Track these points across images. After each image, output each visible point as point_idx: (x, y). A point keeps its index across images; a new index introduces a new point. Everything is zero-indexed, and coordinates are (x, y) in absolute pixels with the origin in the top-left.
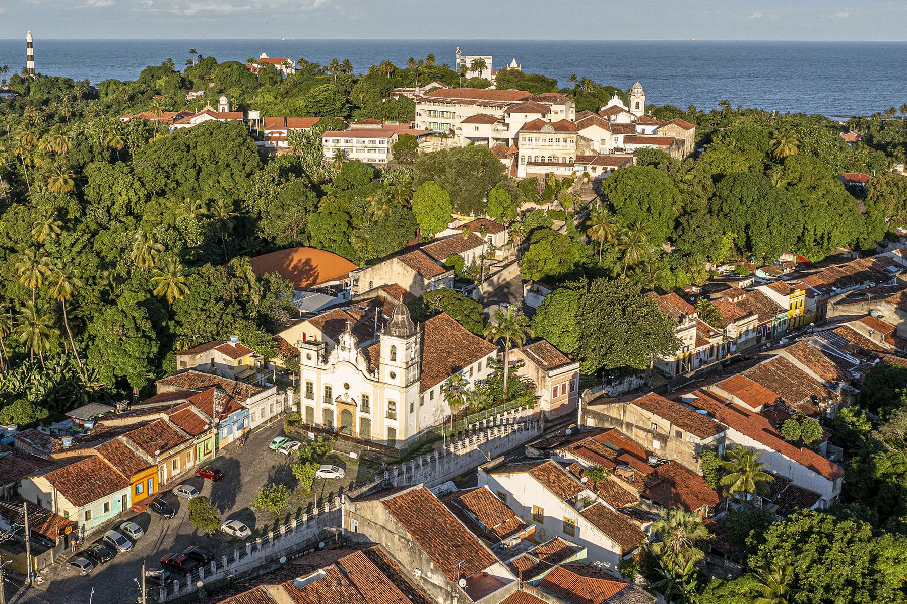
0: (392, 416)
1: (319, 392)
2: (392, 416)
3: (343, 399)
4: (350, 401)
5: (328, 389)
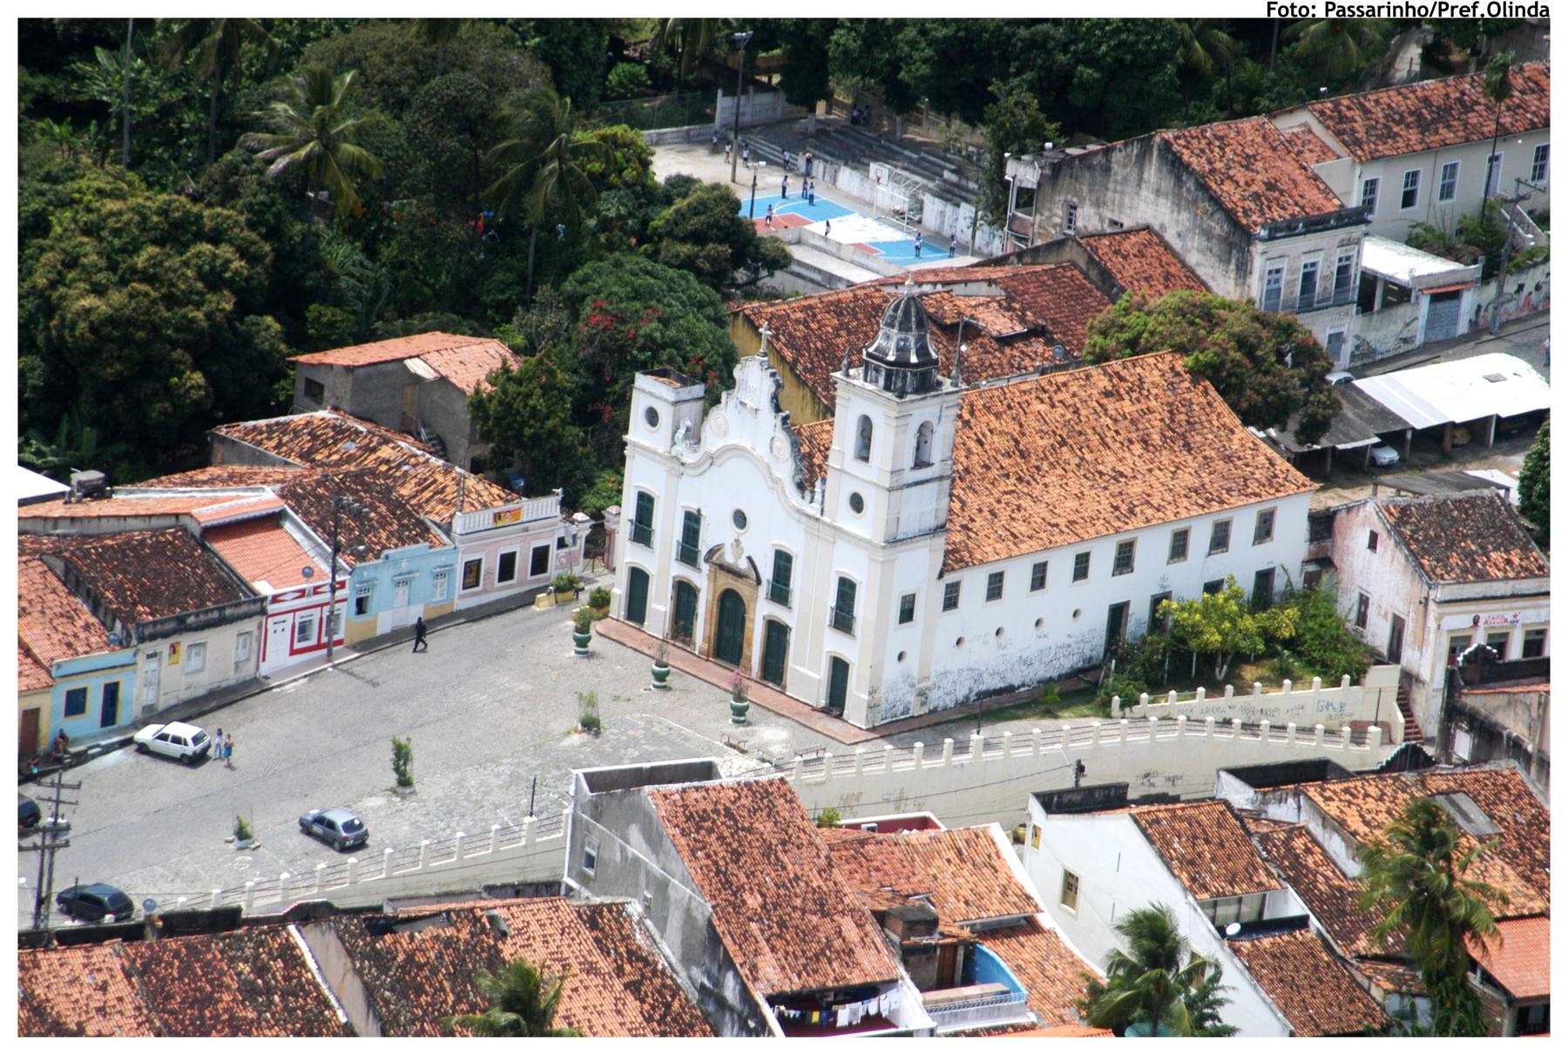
0: (843, 619)
1: (668, 529)
2: (843, 619)
3: (729, 558)
4: (743, 565)
5: (692, 522)
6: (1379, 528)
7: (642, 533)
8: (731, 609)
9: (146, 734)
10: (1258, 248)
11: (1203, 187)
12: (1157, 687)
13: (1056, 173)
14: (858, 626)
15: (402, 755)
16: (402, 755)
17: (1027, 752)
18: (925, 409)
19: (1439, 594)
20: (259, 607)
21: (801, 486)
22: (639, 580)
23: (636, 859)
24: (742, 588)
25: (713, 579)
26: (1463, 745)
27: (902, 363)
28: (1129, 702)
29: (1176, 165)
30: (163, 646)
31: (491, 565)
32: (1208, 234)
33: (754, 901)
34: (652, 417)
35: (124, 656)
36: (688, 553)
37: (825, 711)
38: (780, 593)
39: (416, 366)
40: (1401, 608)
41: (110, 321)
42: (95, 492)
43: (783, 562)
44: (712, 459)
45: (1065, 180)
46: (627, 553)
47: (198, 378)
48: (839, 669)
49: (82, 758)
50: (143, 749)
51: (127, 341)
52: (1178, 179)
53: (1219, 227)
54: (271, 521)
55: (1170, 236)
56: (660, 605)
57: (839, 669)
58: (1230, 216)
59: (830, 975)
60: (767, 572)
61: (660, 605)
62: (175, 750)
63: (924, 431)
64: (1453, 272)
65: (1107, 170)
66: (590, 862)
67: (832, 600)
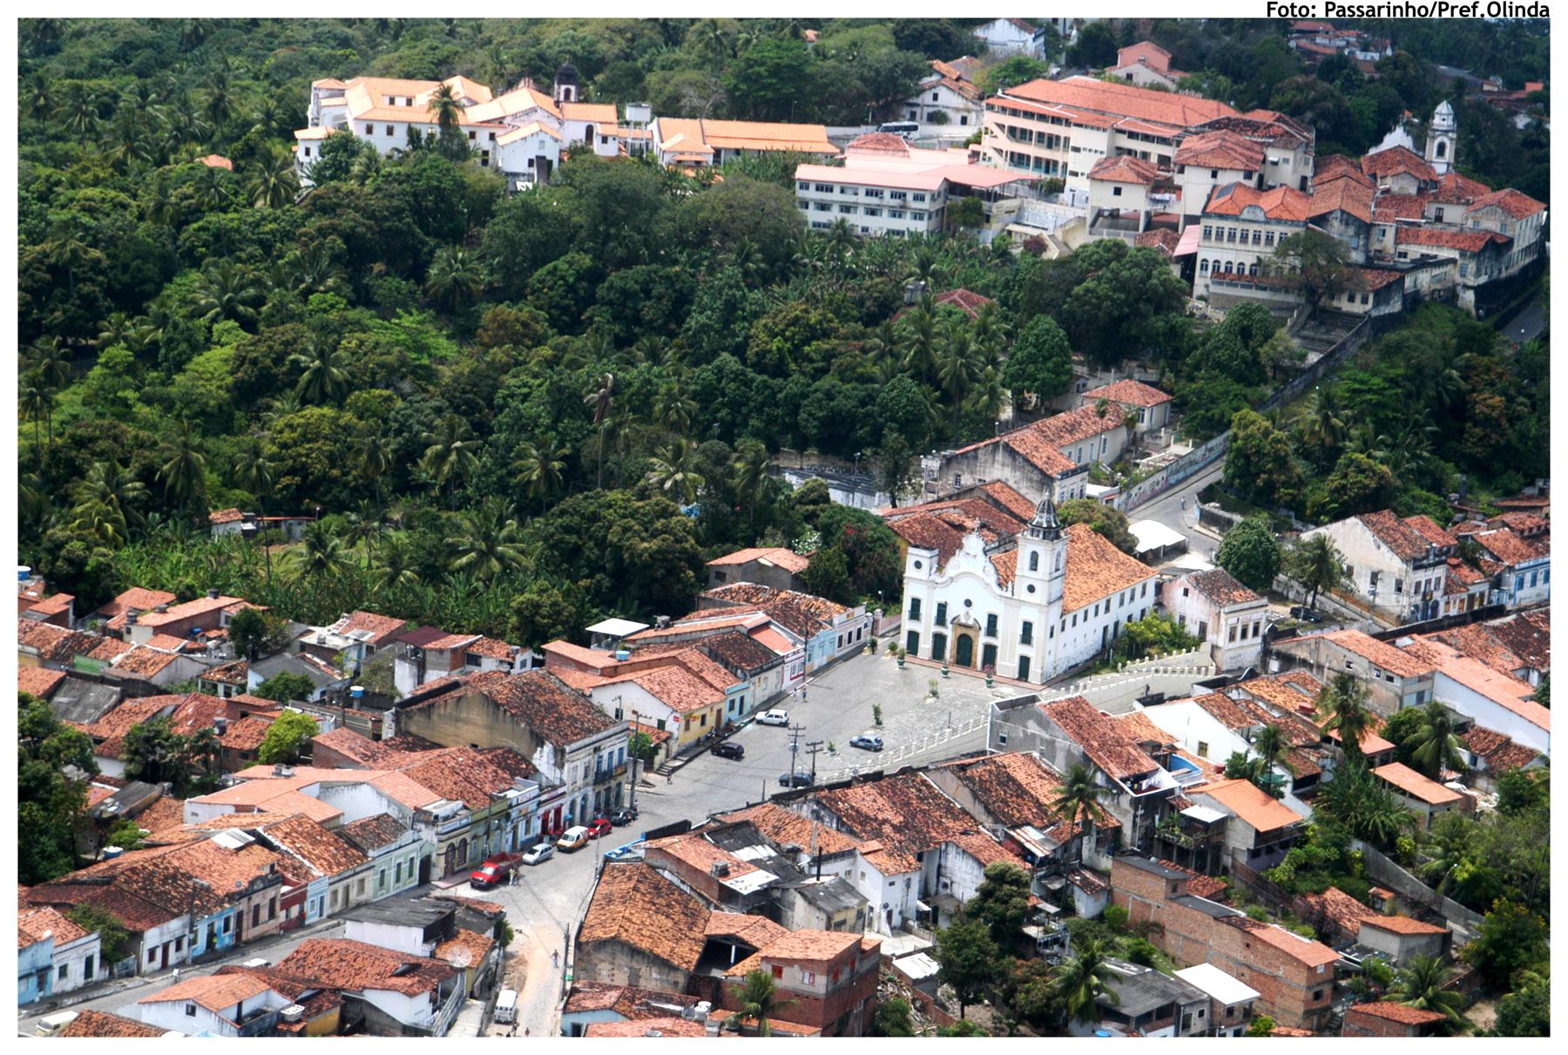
0: (1026, 638)
1: (929, 612)
2: (1026, 638)
3: (963, 621)
4: (971, 622)
5: (942, 609)
6: (1189, 586)
7: (915, 614)
8: (965, 644)
9: (761, 715)
10: (1057, 484)
11: (1027, 460)
12: (1132, 657)
13: (948, 462)
14: (1034, 641)
15: (877, 711)
16: (877, 711)
17: (1104, 688)
18: (1059, 546)
19: (1227, 609)
20: (781, 661)
21: (1000, 585)
22: (913, 637)
23: (1033, 735)
24: (970, 633)
25: (954, 630)
26: (1274, 665)
27: (1049, 527)
28: (1124, 665)
29: (1011, 452)
30: (756, 679)
31: (846, 637)
32: (1031, 480)
33: (1095, 744)
34: (918, 565)
35: (745, 684)
36: (941, 619)
37: (1019, 679)
38: (992, 629)
39: (762, 561)
40: (1204, 619)
41: (658, 552)
42: (667, 625)
43: (992, 620)
44: (952, 579)
45: (954, 464)
46: (907, 625)
47: (691, 573)
48: (1025, 662)
49: (739, 728)
50: (760, 722)
51: (665, 560)
52: (1014, 459)
53: (1036, 476)
54: (765, 626)
55: (1011, 483)
56: (926, 646)
57: (1025, 662)
58: (1041, 471)
59: (1135, 769)
60: (984, 624)
61: (926, 646)
62: (777, 721)
63: (1059, 555)
64: (725, 554)
65: (976, 458)
66: (1003, 740)
67: (1020, 632)
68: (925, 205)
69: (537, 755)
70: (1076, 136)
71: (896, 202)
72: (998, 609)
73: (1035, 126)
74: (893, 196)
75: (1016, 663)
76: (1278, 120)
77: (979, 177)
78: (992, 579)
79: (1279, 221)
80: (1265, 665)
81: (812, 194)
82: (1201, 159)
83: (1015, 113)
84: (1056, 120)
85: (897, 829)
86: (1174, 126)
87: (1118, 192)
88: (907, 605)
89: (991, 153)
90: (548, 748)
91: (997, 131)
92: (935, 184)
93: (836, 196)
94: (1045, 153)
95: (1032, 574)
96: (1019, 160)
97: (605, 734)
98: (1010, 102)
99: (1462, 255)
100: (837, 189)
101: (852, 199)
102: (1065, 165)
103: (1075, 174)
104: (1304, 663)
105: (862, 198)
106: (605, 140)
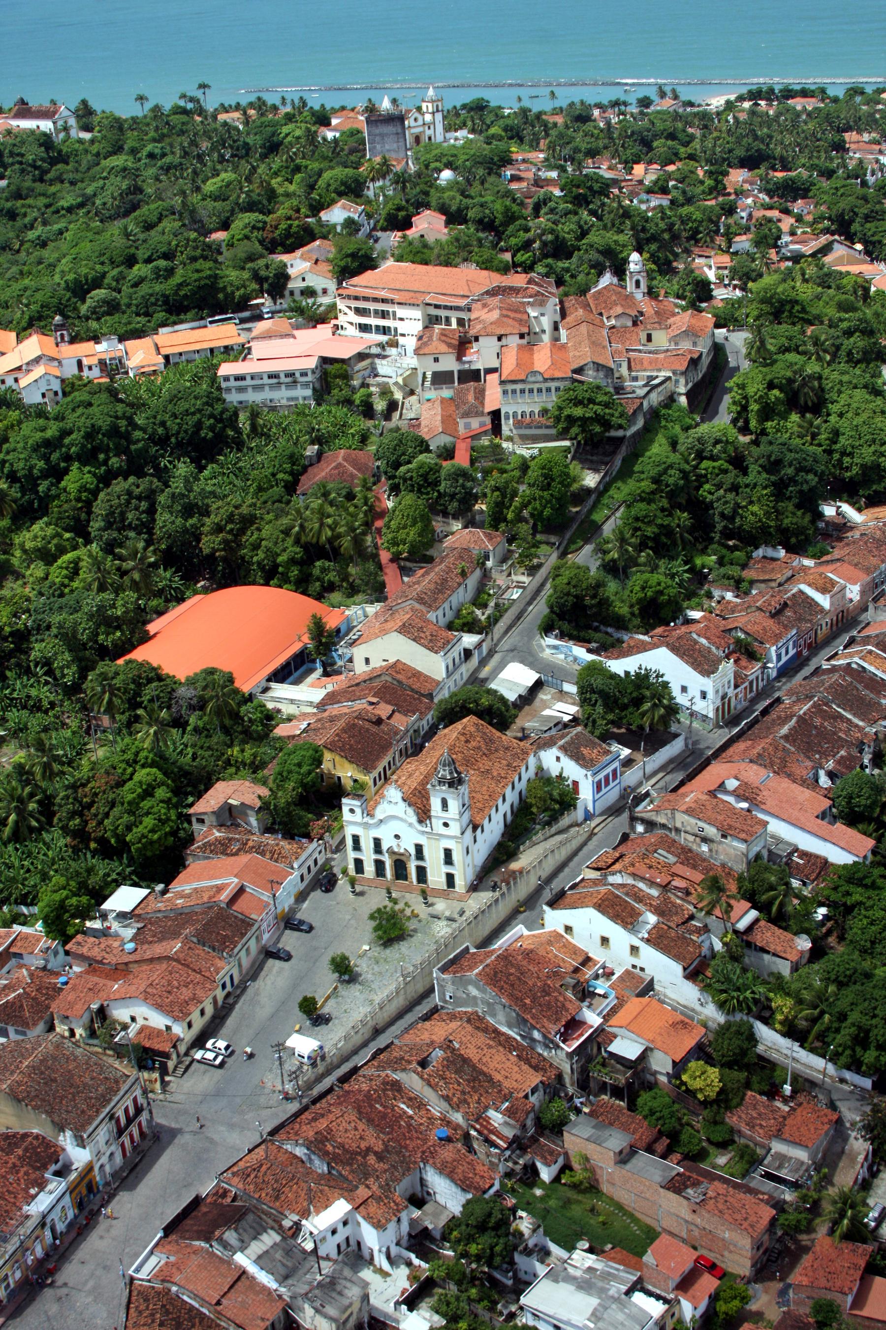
1: (367, 845)
5: (377, 843)
7: (357, 846)
22: (359, 864)
33: (528, 1001)
43: (419, 849)
48: (450, 878)
57: (450, 878)
60: (413, 851)
61: (369, 869)
68: (310, 378)
69: (61, 1138)
70: (401, 312)
71: (289, 380)
72: (422, 840)
73: (372, 306)
74: (286, 376)
75: (443, 879)
76: (529, 282)
77: (343, 351)
78: (413, 819)
79: (553, 379)
80: (633, 828)
81: (232, 383)
82: (489, 330)
83: (356, 298)
84: (384, 301)
85: (380, 1157)
86: (464, 296)
87: (436, 360)
88: (349, 842)
89: (346, 325)
90: (69, 1133)
91: (347, 310)
92: (311, 363)
93: (248, 382)
94: (381, 307)
95: (444, 814)
96: (364, 328)
97: (116, 1099)
98: (352, 291)
99: (674, 373)
100: (248, 378)
101: (260, 382)
102: (396, 329)
103: (403, 335)
104: (664, 826)
105: (266, 380)
106: (90, 368)
